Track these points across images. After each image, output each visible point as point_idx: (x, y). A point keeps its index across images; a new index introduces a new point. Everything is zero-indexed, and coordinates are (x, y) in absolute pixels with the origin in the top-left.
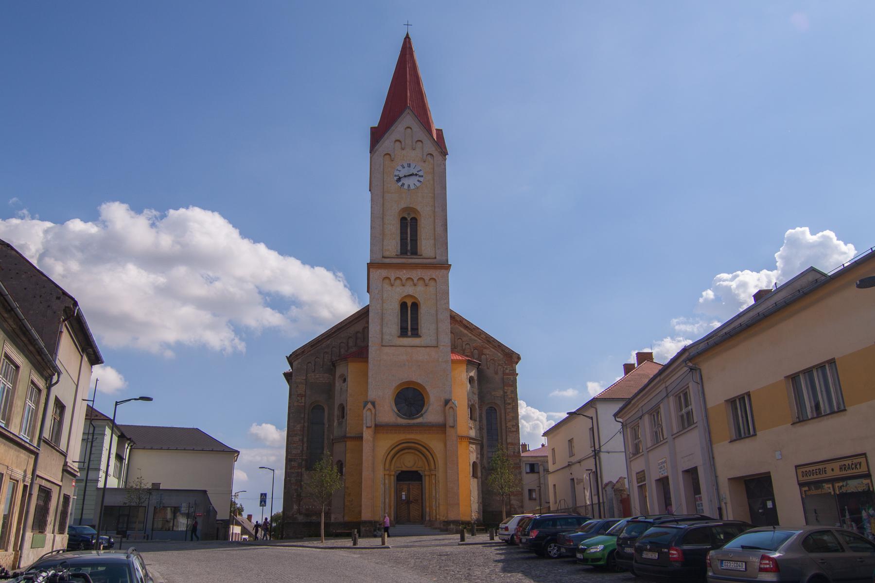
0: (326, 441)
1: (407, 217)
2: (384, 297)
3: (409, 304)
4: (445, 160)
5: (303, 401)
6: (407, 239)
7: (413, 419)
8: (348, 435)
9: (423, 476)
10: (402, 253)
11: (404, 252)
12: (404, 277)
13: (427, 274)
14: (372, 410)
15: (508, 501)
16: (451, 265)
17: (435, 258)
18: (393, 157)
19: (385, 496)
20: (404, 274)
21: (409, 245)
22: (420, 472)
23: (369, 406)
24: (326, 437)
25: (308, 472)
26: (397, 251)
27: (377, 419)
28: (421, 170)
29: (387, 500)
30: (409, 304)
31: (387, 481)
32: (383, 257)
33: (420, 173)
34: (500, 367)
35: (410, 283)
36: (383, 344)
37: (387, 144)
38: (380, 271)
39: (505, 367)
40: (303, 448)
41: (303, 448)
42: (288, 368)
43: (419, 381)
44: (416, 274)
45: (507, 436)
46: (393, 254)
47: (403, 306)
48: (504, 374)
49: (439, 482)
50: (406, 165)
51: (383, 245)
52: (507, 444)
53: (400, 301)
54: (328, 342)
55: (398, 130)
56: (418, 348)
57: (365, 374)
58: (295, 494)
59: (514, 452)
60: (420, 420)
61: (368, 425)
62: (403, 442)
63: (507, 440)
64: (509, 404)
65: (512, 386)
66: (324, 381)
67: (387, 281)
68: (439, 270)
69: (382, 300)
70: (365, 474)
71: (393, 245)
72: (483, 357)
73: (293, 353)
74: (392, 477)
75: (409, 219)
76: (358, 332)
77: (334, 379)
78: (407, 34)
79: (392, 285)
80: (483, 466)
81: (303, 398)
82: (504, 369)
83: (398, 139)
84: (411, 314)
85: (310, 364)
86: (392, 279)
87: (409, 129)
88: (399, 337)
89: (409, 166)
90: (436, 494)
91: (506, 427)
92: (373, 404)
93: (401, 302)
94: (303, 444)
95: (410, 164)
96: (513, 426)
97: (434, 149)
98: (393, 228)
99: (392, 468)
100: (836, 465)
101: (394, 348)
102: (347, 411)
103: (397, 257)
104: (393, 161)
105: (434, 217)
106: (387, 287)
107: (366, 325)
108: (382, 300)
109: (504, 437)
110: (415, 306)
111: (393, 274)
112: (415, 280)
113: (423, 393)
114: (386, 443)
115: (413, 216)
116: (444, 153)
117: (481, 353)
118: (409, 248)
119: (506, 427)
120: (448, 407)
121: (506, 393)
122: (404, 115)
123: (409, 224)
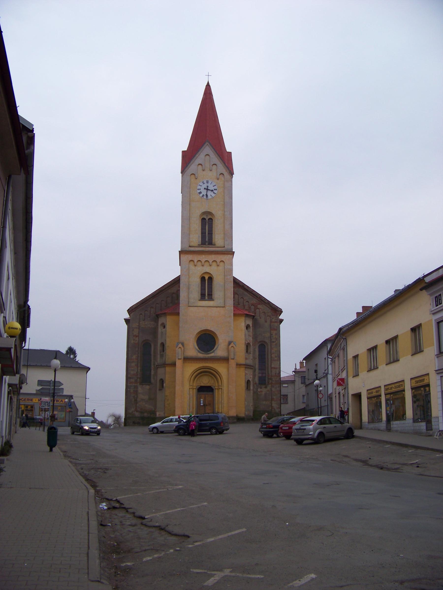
0: (152, 366)
1: (205, 218)
2: (190, 273)
3: (207, 278)
4: (232, 178)
5: (137, 340)
6: (206, 233)
7: (208, 354)
8: (167, 363)
9: (214, 390)
10: (202, 244)
11: (203, 243)
12: (203, 261)
13: (219, 258)
14: (182, 348)
15: (270, 404)
16: (234, 252)
17: (224, 247)
18: (196, 175)
19: (190, 402)
20: (203, 258)
21: (207, 237)
22: (212, 387)
23: (180, 345)
24: (152, 363)
25: (141, 386)
26: (199, 242)
27: (185, 354)
28: (216, 190)
29: (191, 404)
30: (207, 278)
31: (191, 393)
32: (190, 246)
33: (215, 192)
34: (268, 317)
35: (207, 264)
36: (190, 305)
37: (193, 167)
38: (187, 256)
39: (272, 317)
40: (138, 370)
41: (138, 370)
42: (127, 316)
43: (212, 329)
44: (211, 258)
45: (271, 363)
46: (196, 244)
47: (203, 279)
48: (271, 322)
49: (223, 393)
50: (205, 182)
51: (189, 238)
52: (271, 368)
53: (200, 276)
54: (153, 300)
55: (201, 158)
56: (212, 308)
57: (177, 323)
58: (133, 399)
59: (276, 374)
60: (212, 355)
61: (180, 358)
62: (201, 368)
63: (271, 365)
64: (274, 342)
65: (276, 330)
66: (151, 327)
67: (192, 263)
68: (227, 255)
69: (189, 275)
70: (177, 388)
71: (196, 238)
72: (257, 310)
73: (130, 308)
74: (195, 390)
75: (207, 219)
76: (174, 293)
77: (157, 325)
78: (208, 83)
79: (195, 266)
80: (255, 382)
81: (137, 338)
82: (272, 318)
83: (200, 163)
84: (208, 284)
85: (141, 315)
86: (196, 261)
87: (208, 156)
88: (200, 300)
89: (208, 182)
90: (222, 401)
91: (271, 357)
92: (183, 344)
93: (201, 277)
94: (138, 368)
95: (208, 181)
96: (276, 356)
97: (224, 170)
98: (197, 226)
99: (195, 385)
100: (374, 391)
101: (196, 308)
102: (166, 347)
103: (199, 246)
104: (196, 179)
105: (224, 218)
106: (192, 266)
107: (179, 289)
108: (189, 275)
109: (270, 365)
110: (211, 279)
111: (196, 258)
112: (211, 262)
113: (215, 337)
114: (191, 368)
115: (210, 217)
116: (231, 173)
117: (256, 308)
118: (207, 240)
119: (271, 357)
120: (230, 346)
121: (272, 334)
122: (205, 146)
123: (207, 223)
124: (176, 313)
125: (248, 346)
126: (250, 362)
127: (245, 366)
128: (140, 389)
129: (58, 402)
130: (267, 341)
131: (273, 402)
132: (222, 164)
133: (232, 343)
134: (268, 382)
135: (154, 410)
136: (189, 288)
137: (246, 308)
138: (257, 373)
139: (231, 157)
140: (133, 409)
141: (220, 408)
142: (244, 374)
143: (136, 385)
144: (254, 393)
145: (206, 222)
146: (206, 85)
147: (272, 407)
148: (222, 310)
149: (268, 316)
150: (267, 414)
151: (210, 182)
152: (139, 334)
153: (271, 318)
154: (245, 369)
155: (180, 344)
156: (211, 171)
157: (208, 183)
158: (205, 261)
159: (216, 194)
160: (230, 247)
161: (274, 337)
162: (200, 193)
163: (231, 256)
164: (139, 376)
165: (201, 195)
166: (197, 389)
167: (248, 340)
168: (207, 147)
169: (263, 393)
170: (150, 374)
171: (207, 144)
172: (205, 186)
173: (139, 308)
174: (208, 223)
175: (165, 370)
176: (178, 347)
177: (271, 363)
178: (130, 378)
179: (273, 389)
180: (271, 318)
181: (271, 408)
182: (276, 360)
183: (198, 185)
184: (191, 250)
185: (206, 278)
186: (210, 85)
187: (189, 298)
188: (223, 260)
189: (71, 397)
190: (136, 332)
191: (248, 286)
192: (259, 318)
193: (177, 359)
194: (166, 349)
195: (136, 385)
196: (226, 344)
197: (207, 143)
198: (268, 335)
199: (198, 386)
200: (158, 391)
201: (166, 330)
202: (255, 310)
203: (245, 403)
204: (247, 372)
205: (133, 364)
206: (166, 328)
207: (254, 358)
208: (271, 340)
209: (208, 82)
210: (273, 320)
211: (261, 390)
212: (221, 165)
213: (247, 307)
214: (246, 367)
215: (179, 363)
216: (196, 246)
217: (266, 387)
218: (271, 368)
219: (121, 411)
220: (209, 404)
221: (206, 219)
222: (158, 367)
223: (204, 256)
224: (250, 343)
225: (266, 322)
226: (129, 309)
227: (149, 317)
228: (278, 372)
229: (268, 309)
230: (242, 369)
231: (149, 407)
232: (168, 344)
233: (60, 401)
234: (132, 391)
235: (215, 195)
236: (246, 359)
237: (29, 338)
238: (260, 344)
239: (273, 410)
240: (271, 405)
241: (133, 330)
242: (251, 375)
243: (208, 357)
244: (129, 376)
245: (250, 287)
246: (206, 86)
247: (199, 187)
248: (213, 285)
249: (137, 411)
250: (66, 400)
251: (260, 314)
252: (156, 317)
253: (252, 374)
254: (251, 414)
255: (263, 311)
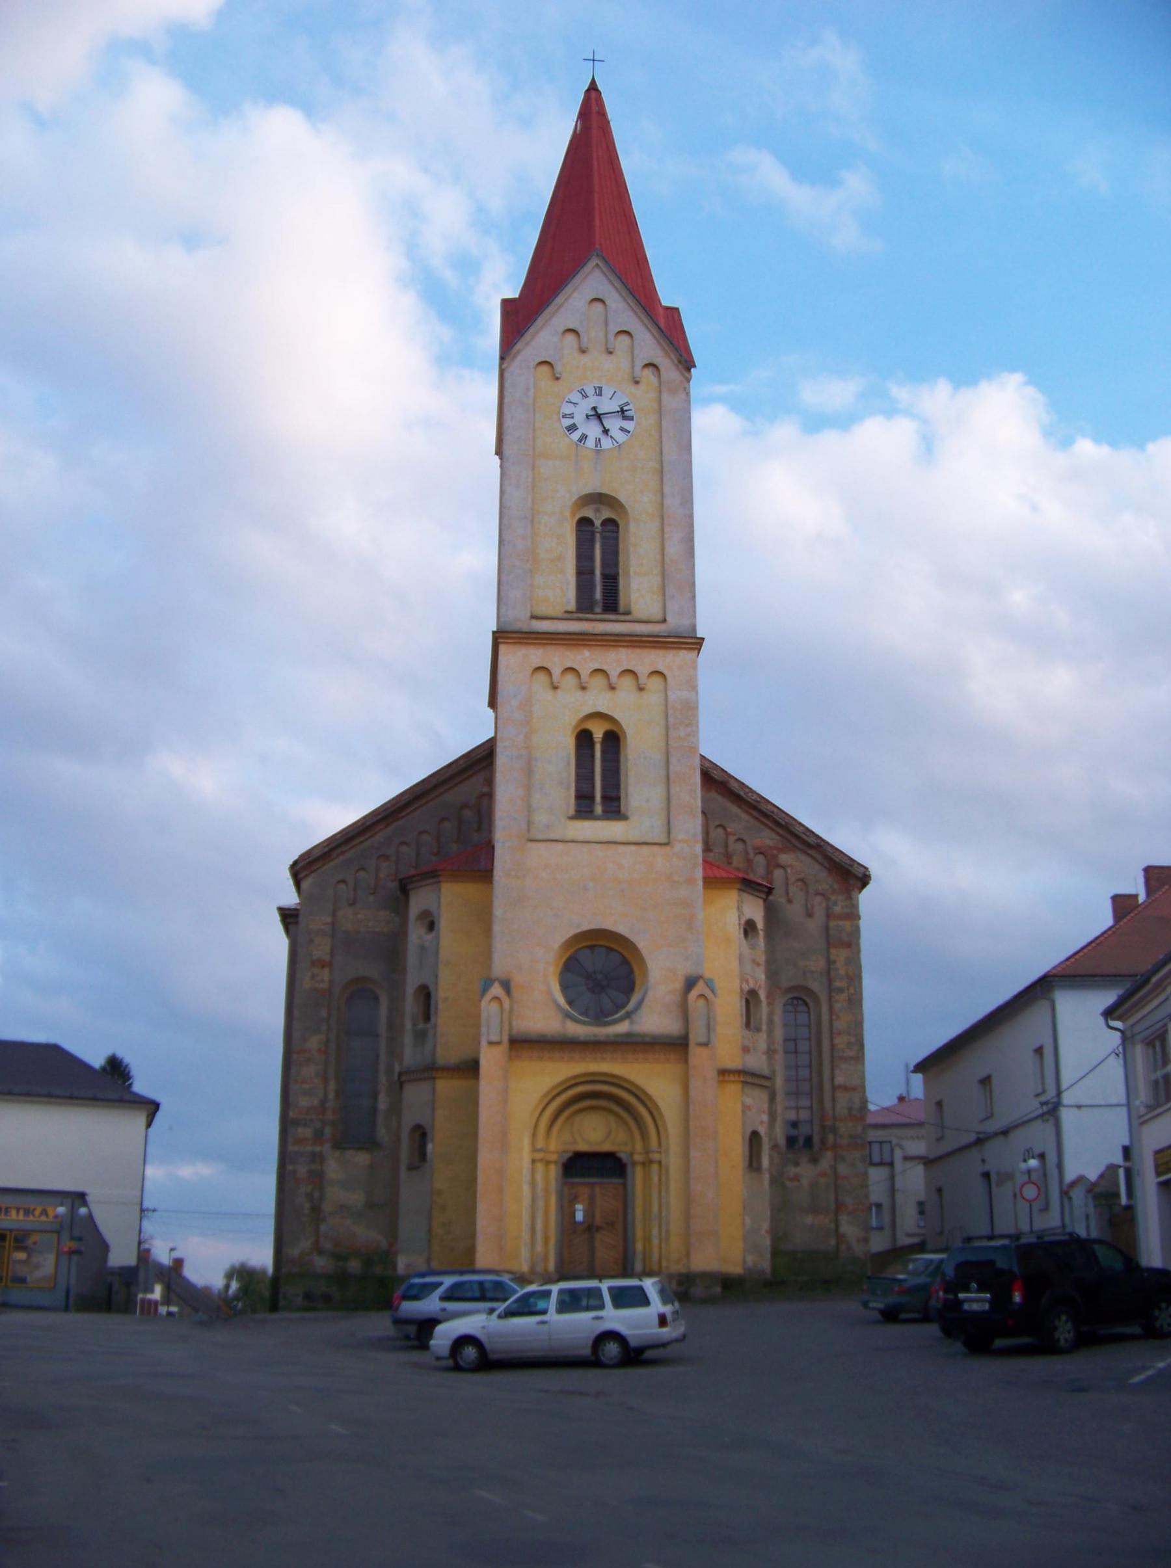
0: (383, 1079)
3: (598, 735)
4: (688, 380)
5: (326, 978)
9: (629, 1169)
11: (585, 604)
13: (645, 661)
15: (833, 1226)
16: (703, 639)
17: (664, 621)
20: (586, 659)
22: (623, 1156)
23: (496, 990)
24: (382, 1067)
30: (598, 735)
31: (539, 1177)
32: (534, 617)
36: (536, 834)
39: (833, 898)
44: (615, 660)
45: (832, 1069)
46: (558, 611)
47: (584, 738)
48: (829, 916)
50: (590, 391)
52: (834, 1088)
53: (576, 727)
57: (483, 919)
58: (307, 1205)
59: (850, 1109)
60: (623, 1028)
61: (494, 1038)
64: (841, 990)
70: (485, 1157)
74: (553, 1167)
75: (598, 523)
76: (465, 806)
79: (555, 688)
83: (571, 327)
87: (598, 307)
88: (572, 818)
89: (599, 392)
91: (833, 1047)
92: (506, 985)
93: (578, 730)
95: (601, 388)
101: (560, 846)
103: (568, 616)
107: (485, 790)
109: (827, 1074)
110: (614, 739)
111: (557, 658)
115: (607, 514)
116: (687, 363)
117: (773, 864)
119: (833, 1047)
120: (694, 993)
121: (834, 962)
123: (598, 536)
124: (478, 871)
125: (750, 999)
126: (757, 1062)
127: (742, 1079)
128: (333, 1169)
129: (31, 1218)
130: (816, 986)
131: (844, 1218)
132: (650, 330)
133: (701, 984)
134: (823, 1141)
135: (384, 1245)
136: (529, 772)
137: (735, 864)
138: (779, 1109)
139: (680, 320)
140: (305, 1244)
141: (655, 1242)
142: (739, 1107)
143: (318, 1149)
144: (774, 1180)
145: (593, 533)
146: (586, 88)
147: (840, 1237)
148: (659, 858)
149: (818, 893)
150: (975, 1285)
151: (567, 422)
152: (332, 953)
153: (828, 899)
154: (742, 1090)
155: (496, 984)
156: (611, 353)
157: (600, 394)
158: (591, 670)
159: (629, 432)
160: (686, 622)
161: (842, 972)
162: (572, 428)
163: (691, 655)
164: (330, 1116)
165: (576, 436)
166: (560, 1166)
167: (750, 980)
168: (597, 274)
169: (805, 1182)
170: (374, 1110)
171: (597, 265)
172: (585, 407)
173: (334, 859)
174: (603, 538)
175: (434, 1090)
176: (488, 996)
177: (832, 1069)
178: (296, 1123)
179: (843, 1169)
180: (828, 899)
181: (833, 1242)
182: (851, 1058)
183: (564, 402)
184: (541, 631)
185: (595, 736)
186: (600, 88)
187: (529, 809)
188: (660, 668)
189: (81, 1197)
190: (322, 948)
191: (743, 784)
192: (783, 900)
193: (484, 1043)
194: (436, 1008)
195: (318, 1149)
196: (678, 985)
197: (595, 261)
198: (817, 963)
199: (564, 1152)
200: (403, 1174)
201: (438, 938)
202: (769, 872)
203: (744, 1219)
204: (748, 1101)
205: (309, 1071)
206: (439, 930)
207: (770, 1052)
208: (830, 981)
209: (593, 78)
210: (838, 909)
211: (798, 1170)
212: (647, 336)
213: (737, 861)
214: (744, 1083)
215: (490, 1060)
216: (560, 615)
217: (814, 1160)
218: (834, 1088)
219: (262, 1256)
220: (607, 1224)
221: (595, 521)
222: (404, 1078)
223: (587, 653)
224: (757, 989)
225: (810, 915)
226: (295, 863)
227: (372, 891)
228: (857, 1104)
229: (817, 866)
230: (733, 1089)
231: (366, 1234)
232: (443, 993)
233: (37, 1213)
234: (302, 1170)
235: (625, 439)
236: (746, 1050)
237: (597, 1321)
238: (790, 996)
239: (843, 1247)
240: (837, 1226)
241: (311, 941)
242: (764, 1112)
243: (608, 1036)
244: (292, 1114)
245: (750, 786)
246: (588, 91)
247: (567, 409)
248: (622, 760)
249: (321, 1252)
250: (61, 1210)
251: (787, 885)
252: (399, 893)
253: (766, 1110)
254: (766, 1265)
255: (799, 876)
